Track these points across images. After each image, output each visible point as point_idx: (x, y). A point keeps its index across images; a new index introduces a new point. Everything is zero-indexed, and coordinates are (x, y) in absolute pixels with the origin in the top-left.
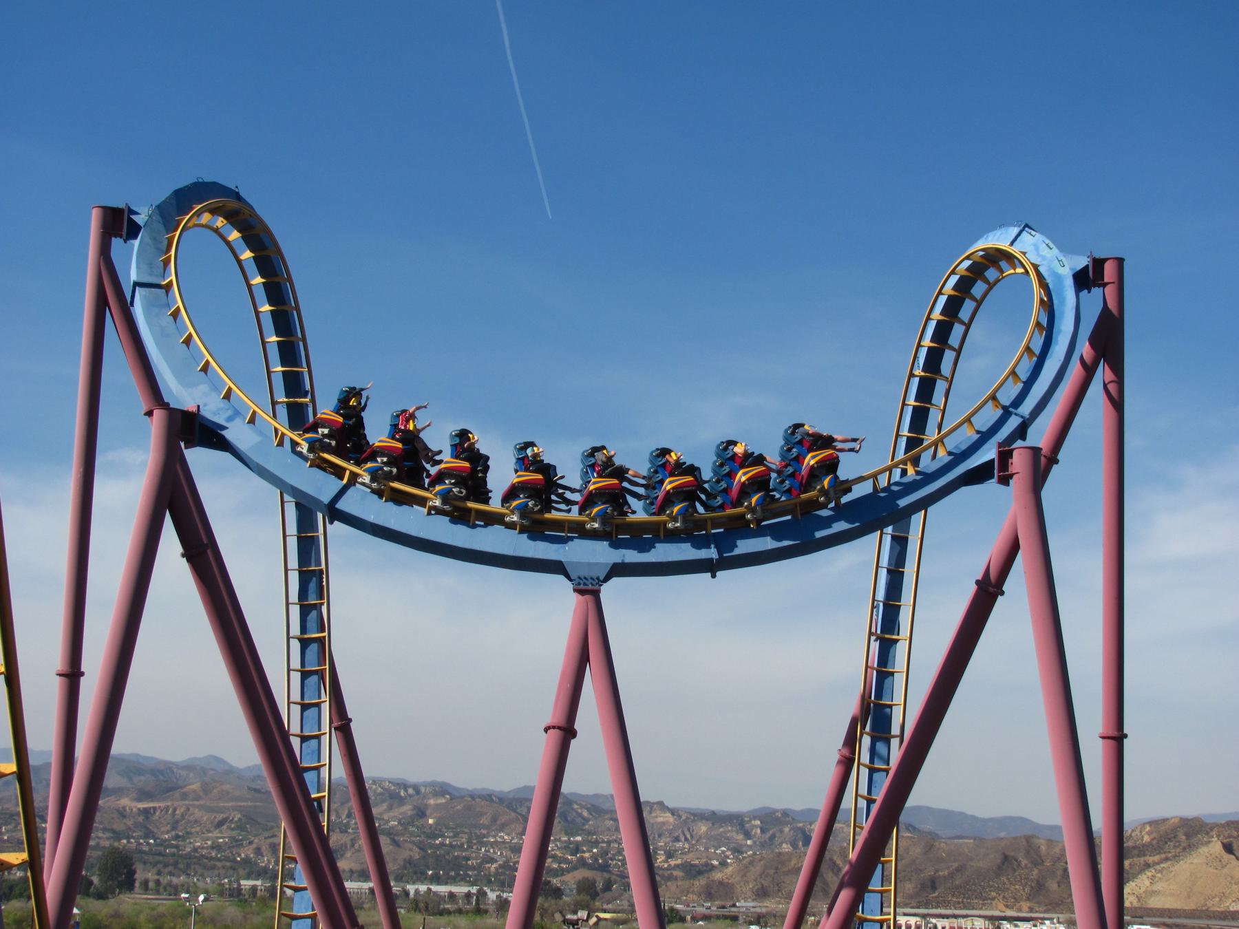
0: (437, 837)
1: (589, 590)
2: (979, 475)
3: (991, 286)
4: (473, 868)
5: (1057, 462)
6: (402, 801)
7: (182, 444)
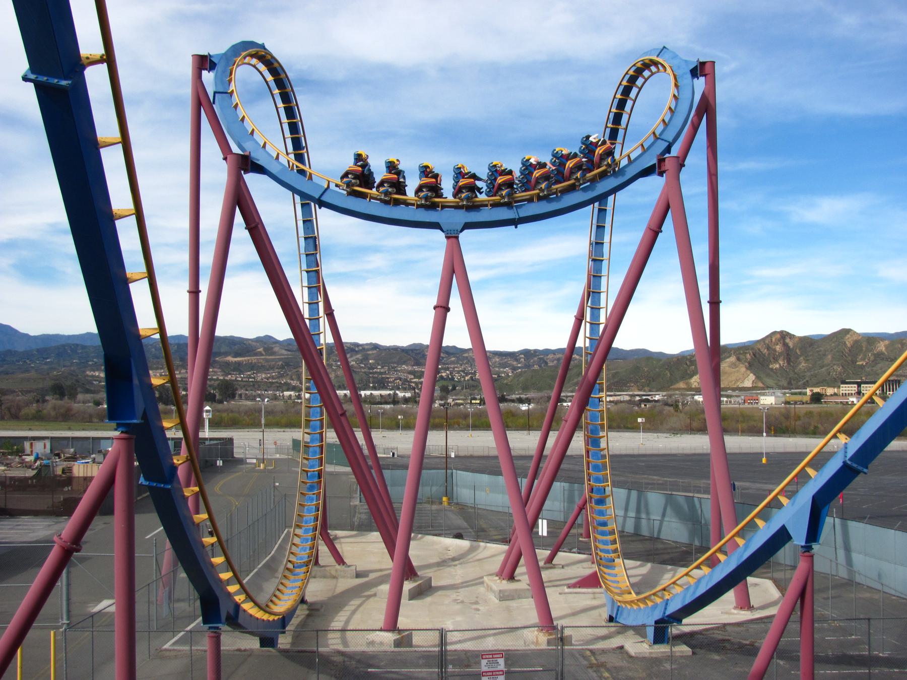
0: (374, 369)
1: (453, 237)
2: (647, 172)
3: (653, 74)
4: (391, 382)
5: (684, 166)
6: (357, 352)
7: (242, 172)
